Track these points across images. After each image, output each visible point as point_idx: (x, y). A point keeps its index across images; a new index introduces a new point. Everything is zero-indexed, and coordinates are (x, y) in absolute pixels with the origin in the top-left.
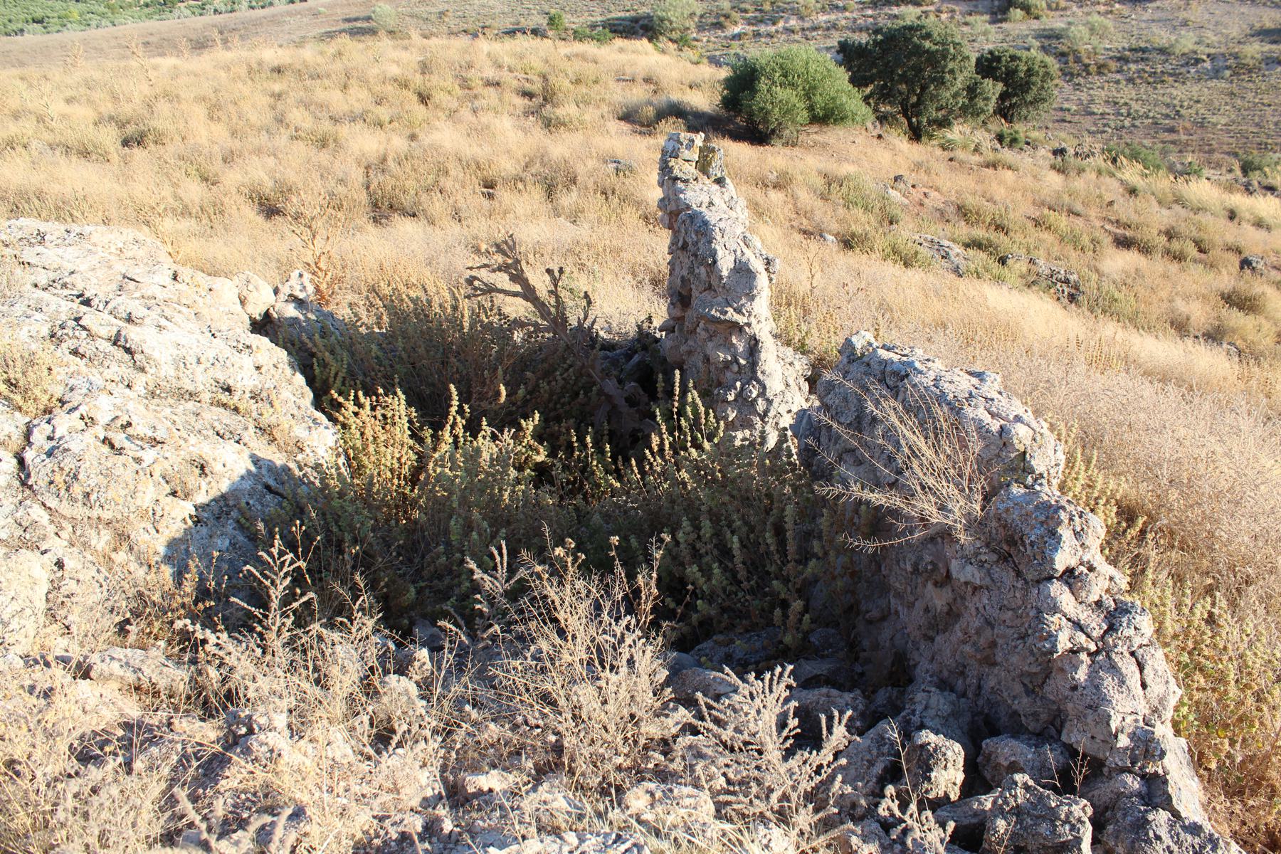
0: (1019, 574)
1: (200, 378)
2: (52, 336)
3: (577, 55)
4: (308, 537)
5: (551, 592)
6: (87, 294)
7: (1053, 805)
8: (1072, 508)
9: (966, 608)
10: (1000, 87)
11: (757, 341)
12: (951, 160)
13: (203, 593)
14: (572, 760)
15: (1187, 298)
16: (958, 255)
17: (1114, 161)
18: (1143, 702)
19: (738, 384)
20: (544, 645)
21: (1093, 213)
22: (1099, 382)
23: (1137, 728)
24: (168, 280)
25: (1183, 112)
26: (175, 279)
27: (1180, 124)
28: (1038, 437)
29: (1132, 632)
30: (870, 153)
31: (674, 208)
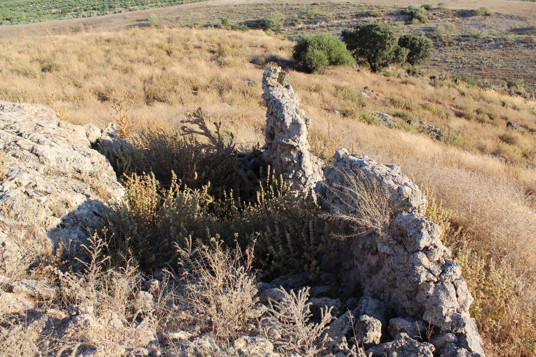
0: (405, 249)
1: (68, 167)
2: (5, 149)
3: (233, 36)
4: (109, 233)
5: (208, 256)
6: (21, 132)
7: (417, 346)
8: (427, 221)
9: (384, 264)
10: (408, 51)
11: (301, 153)
12: (388, 80)
13: (65, 256)
14: (216, 327)
15: (485, 138)
16: (390, 120)
17: (456, 81)
18: (457, 303)
19: (294, 171)
20: (206, 279)
21: (446, 103)
22: (446, 170)
23: (454, 314)
24: (56, 126)
25: (484, 62)
26: (59, 126)
27: (482, 67)
28: (414, 192)
29: (452, 273)
30: (354, 77)
31: (268, 98)
